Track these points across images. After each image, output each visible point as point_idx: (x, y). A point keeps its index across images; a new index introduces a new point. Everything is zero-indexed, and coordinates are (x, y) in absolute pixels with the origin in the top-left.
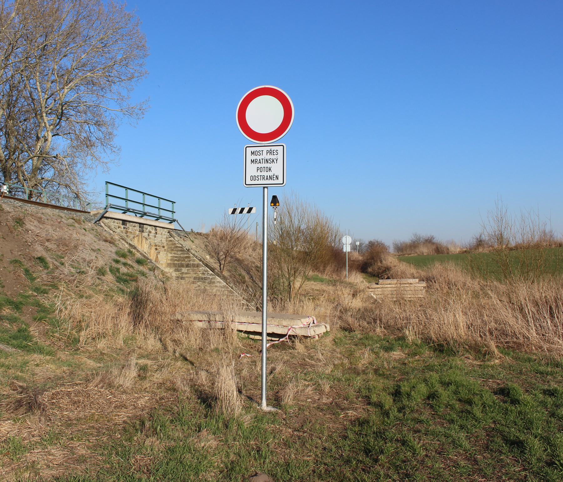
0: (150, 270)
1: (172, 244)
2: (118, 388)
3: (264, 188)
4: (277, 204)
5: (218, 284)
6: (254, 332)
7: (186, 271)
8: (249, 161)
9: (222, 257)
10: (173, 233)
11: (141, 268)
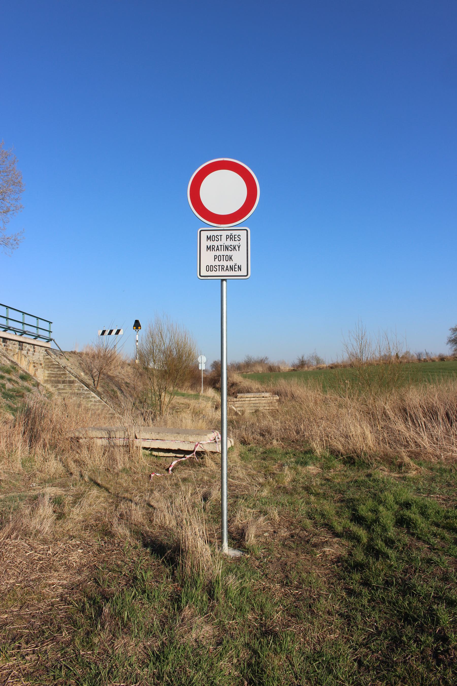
0: (34, 385)
1: (49, 362)
2: (35, 535)
3: (222, 280)
4: (139, 328)
5: (93, 399)
6: (164, 449)
7: (62, 387)
8: (204, 248)
9: (95, 374)
10: (50, 352)
11: (26, 384)
